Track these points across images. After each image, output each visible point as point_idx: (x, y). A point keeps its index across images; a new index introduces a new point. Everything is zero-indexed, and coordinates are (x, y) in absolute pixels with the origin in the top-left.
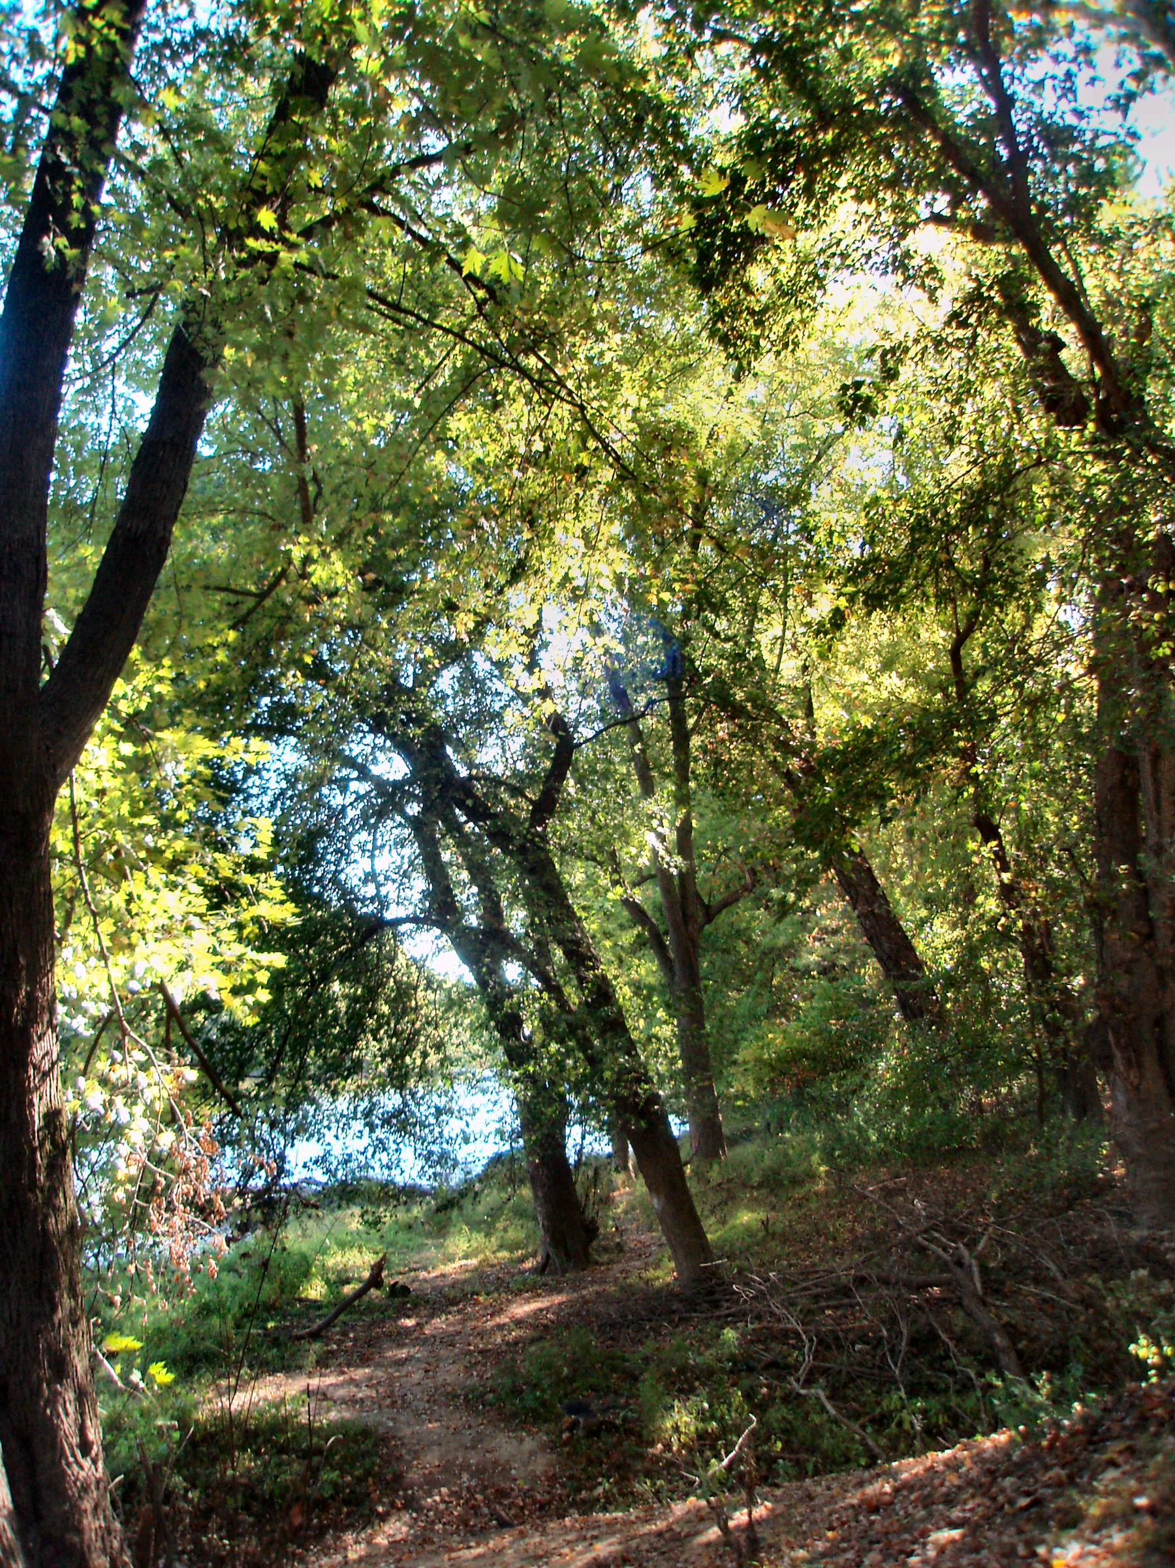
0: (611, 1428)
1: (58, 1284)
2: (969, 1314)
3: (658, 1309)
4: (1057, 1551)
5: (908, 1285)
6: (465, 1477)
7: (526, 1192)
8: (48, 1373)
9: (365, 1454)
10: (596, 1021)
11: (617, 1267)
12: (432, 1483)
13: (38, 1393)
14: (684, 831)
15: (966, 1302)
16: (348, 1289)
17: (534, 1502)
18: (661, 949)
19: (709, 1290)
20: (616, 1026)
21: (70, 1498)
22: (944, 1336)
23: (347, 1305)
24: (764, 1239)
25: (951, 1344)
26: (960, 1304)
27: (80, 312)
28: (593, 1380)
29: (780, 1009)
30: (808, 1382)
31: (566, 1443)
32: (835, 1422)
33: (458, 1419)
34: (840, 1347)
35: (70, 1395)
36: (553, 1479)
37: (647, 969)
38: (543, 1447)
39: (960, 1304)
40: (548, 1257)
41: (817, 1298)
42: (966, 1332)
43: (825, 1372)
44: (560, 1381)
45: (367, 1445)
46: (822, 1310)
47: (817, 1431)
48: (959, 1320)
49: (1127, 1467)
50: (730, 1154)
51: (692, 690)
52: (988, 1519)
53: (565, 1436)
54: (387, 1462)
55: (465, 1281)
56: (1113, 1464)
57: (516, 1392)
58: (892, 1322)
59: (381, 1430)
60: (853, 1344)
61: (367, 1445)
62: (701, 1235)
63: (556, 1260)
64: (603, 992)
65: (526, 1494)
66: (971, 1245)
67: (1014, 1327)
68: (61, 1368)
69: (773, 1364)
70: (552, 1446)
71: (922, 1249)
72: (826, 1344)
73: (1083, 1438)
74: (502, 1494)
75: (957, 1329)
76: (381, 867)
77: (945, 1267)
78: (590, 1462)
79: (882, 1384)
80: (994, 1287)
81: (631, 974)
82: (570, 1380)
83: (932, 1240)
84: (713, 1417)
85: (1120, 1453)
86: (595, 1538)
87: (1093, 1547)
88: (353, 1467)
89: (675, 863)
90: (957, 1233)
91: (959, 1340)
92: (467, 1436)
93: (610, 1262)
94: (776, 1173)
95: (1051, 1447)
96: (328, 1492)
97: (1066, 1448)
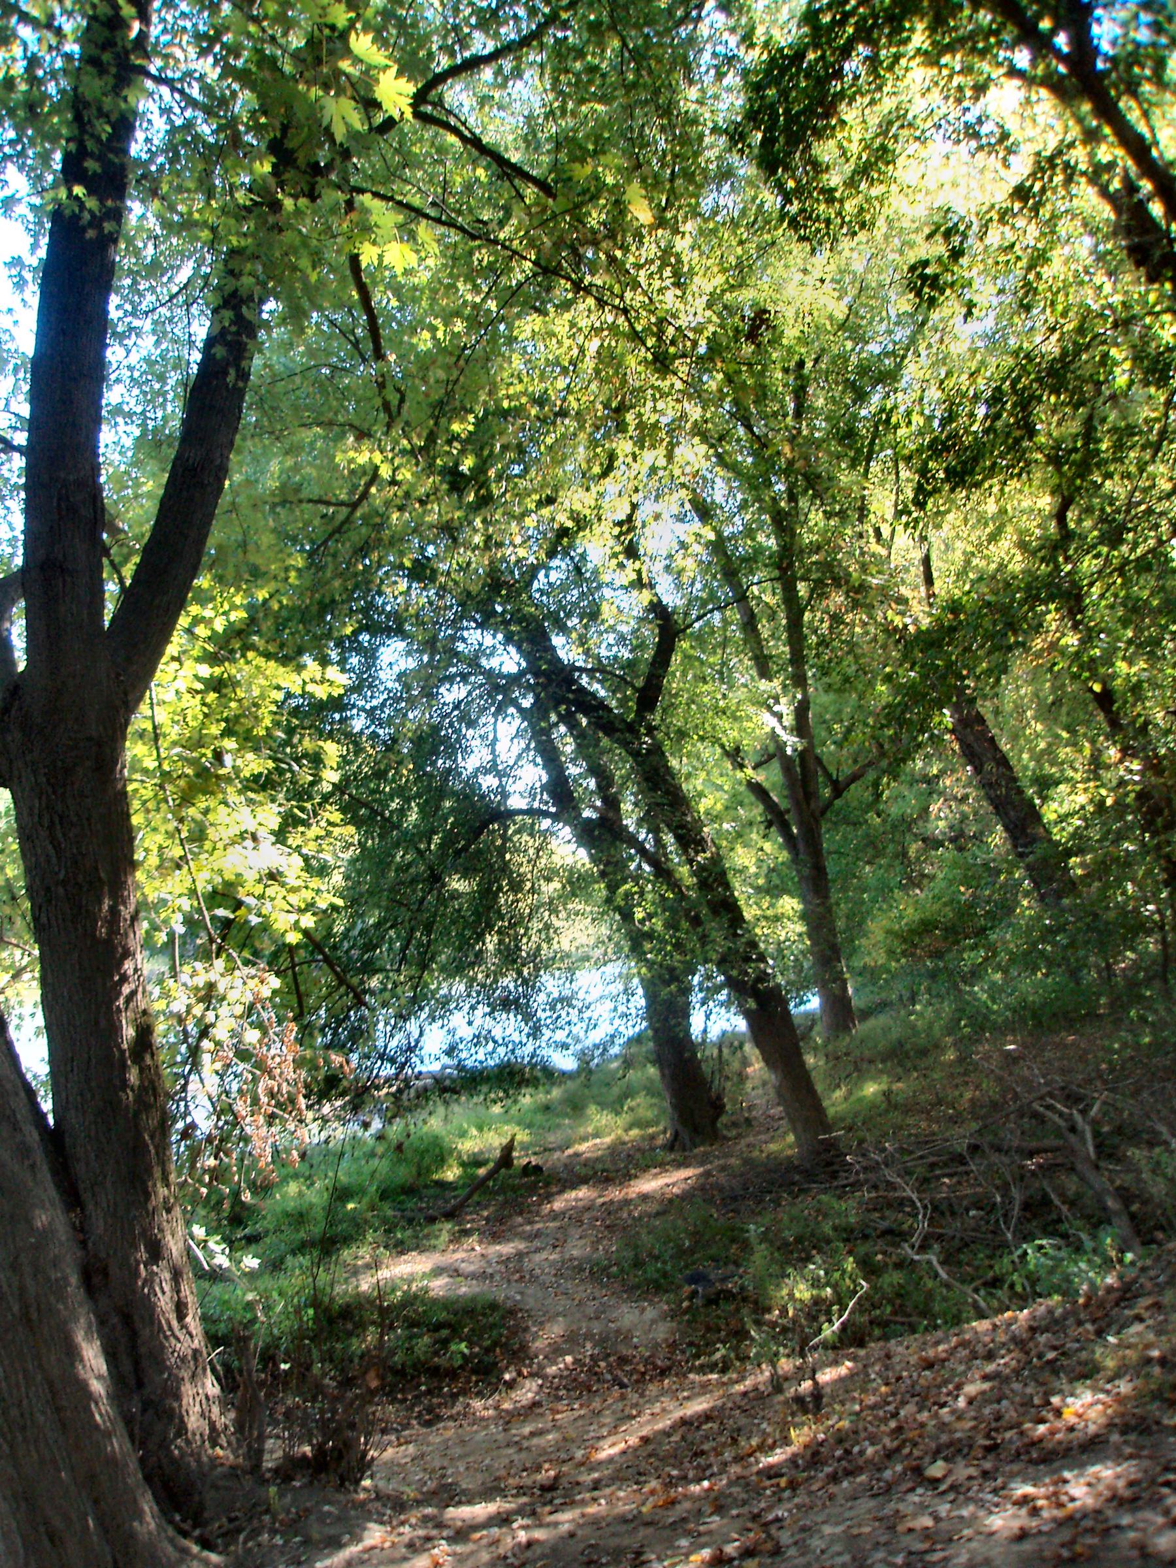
0: (729, 1296)
1: (151, 1175)
2: (1082, 1179)
3: (781, 1180)
4: (1070, 1400)
5: (1019, 1150)
6: (589, 1345)
7: (652, 1071)
8: (145, 1256)
9: (493, 1326)
10: (712, 902)
11: (743, 1142)
12: (556, 1352)
13: (137, 1274)
14: (801, 711)
15: (1079, 1167)
16: (482, 1171)
17: (655, 1367)
18: (785, 829)
19: (824, 1163)
20: (729, 910)
21: (169, 1369)
22: (1057, 1202)
23: (479, 1185)
24: (887, 1111)
25: (1064, 1208)
26: (1073, 1169)
27: (114, 300)
28: (713, 1251)
29: (916, 881)
30: (923, 1248)
31: (685, 1312)
32: (948, 1286)
33: (583, 1291)
34: (953, 1214)
35: (166, 1275)
36: (673, 1346)
37: (773, 848)
38: (664, 1317)
39: (1073, 1169)
40: (676, 1135)
41: (933, 1166)
42: (1079, 1196)
43: (940, 1238)
44: (681, 1252)
45: (495, 1318)
46: (938, 1178)
47: (930, 1295)
48: (1072, 1185)
49: (1150, 1322)
50: (860, 1029)
51: (785, 574)
52: (1017, 1372)
53: (685, 1304)
54: (514, 1332)
55: (597, 1159)
56: (1139, 1319)
57: (638, 1264)
58: (1005, 1189)
59: (509, 1304)
60: (967, 1210)
61: (495, 1318)
62: (819, 1109)
63: (685, 1136)
64: (714, 878)
65: (646, 1361)
66: (1083, 1112)
67: (1126, 1189)
68: (156, 1252)
69: (889, 1232)
70: (673, 1315)
71: (1035, 1115)
72: (938, 1211)
73: (1116, 1295)
74: (623, 1360)
75: (1070, 1193)
76: (503, 756)
77: (1059, 1134)
78: (708, 1329)
79: (996, 1248)
80: (1106, 1150)
81: (752, 856)
82: (692, 1251)
83: (1049, 1107)
84: (828, 1284)
85: (1147, 1308)
86: (687, 1398)
87: (1101, 1396)
88: (481, 1337)
89: (792, 743)
90: (1072, 1099)
91: (1072, 1204)
92: (591, 1308)
93: (739, 1136)
94: (901, 1044)
95: (1086, 1305)
96: (459, 1362)
97: (1101, 1305)
